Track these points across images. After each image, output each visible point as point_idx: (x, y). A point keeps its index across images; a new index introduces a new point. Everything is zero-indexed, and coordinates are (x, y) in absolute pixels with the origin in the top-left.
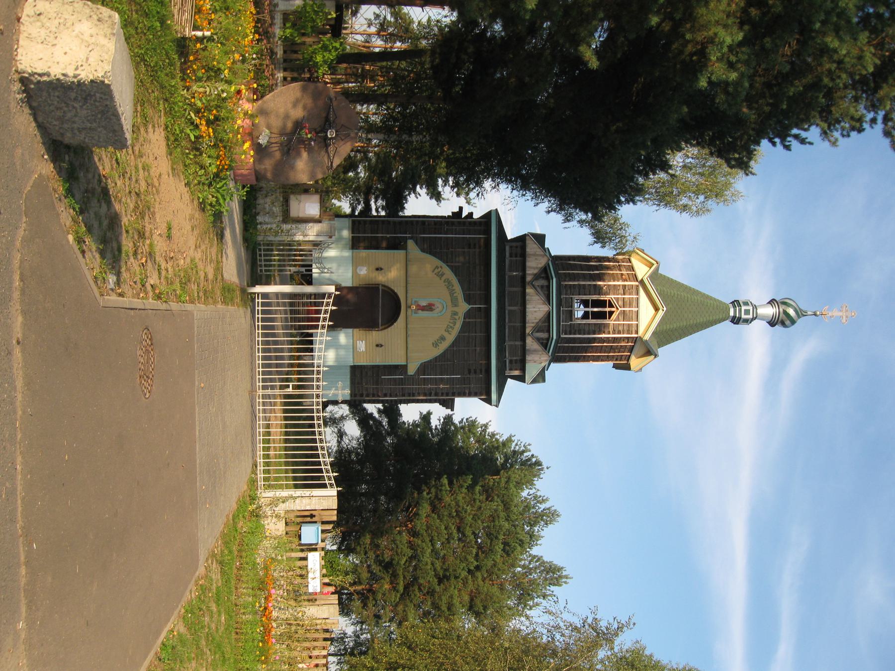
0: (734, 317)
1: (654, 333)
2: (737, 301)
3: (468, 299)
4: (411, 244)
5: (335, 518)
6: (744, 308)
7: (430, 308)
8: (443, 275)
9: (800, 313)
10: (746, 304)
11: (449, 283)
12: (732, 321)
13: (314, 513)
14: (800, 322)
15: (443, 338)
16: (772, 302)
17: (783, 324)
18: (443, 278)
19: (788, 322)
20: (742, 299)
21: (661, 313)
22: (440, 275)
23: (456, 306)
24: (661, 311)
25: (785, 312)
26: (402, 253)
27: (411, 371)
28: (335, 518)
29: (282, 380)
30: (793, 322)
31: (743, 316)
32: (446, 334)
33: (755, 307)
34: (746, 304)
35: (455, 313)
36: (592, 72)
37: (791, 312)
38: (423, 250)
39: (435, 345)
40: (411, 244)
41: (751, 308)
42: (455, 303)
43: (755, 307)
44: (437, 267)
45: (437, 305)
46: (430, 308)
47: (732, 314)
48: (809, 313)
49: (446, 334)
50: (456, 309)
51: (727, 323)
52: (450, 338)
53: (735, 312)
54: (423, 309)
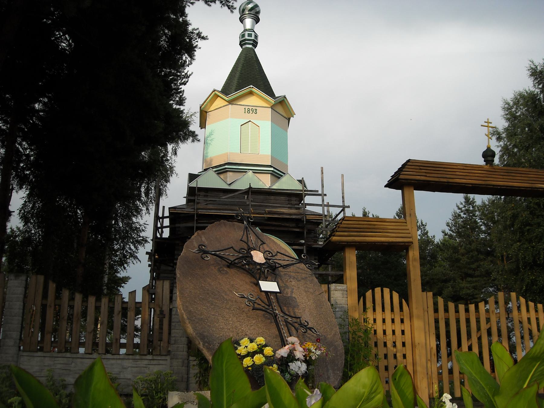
0: (252, 44)
2: (241, 42)
5: (41, 278)
12: (255, 47)
16: (242, 20)
17: (258, 12)
21: (255, 90)
28: (41, 278)
30: (256, 6)
33: (245, 30)
36: (80, 292)
37: (250, 6)
41: (247, 33)
43: (245, 30)
47: (251, 46)
48: (219, 102)
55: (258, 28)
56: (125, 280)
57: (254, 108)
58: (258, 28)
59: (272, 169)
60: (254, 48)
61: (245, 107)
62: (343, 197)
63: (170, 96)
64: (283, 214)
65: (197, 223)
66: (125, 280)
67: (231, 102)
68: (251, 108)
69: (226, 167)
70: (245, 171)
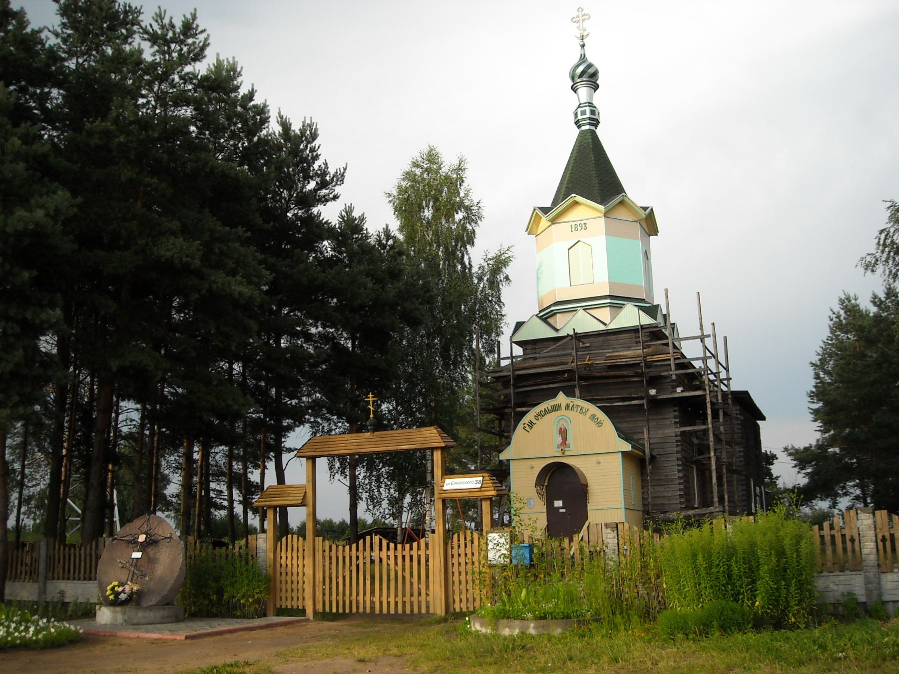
1: (601, 203)
3: (553, 394)
4: (503, 456)
6: (580, 117)
7: (563, 433)
8: (531, 422)
9: (583, 59)
10: (576, 114)
11: (539, 415)
13: (880, 537)
14: (591, 59)
15: (593, 417)
18: (534, 421)
19: (591, 71)
20: (573, 121)
21: (579, 198)
22: (531, 424)
23: (560, 406)
24: (576, 199)
25: (581, 75)
26: (513, 467)
27: (627, 447)
29: (22, 565)
30: (590, 66)
31: (588, 115)
32: (589, 414)
34: (576, 114)
35: (567, 407)
37: (581, 69)
38: (509, 443)
39: (599, 424)
40: (503, 456)
42: (556, 408)
44: (524, 428)
45: (560, 425)
46: (563, 433)
49: (589, 414)
50: (563, 407)
51: (600, 131)
52: (593, 409)
53: (585, 124)
54: (565, 439)
55: (598, 99)
56: (433, 195)
57: (582, 222)
58: (598, 99)
59: (608, 301)
60: (593, 128)
61: (570, 224)
62: (701, 325)
63: (868, 315)
64: (626, 357)
65: (515, 387)
66: (433, 195)
67: (553, 221)
68: (578, 223)
69: (552, 308)
70: (574, 310)
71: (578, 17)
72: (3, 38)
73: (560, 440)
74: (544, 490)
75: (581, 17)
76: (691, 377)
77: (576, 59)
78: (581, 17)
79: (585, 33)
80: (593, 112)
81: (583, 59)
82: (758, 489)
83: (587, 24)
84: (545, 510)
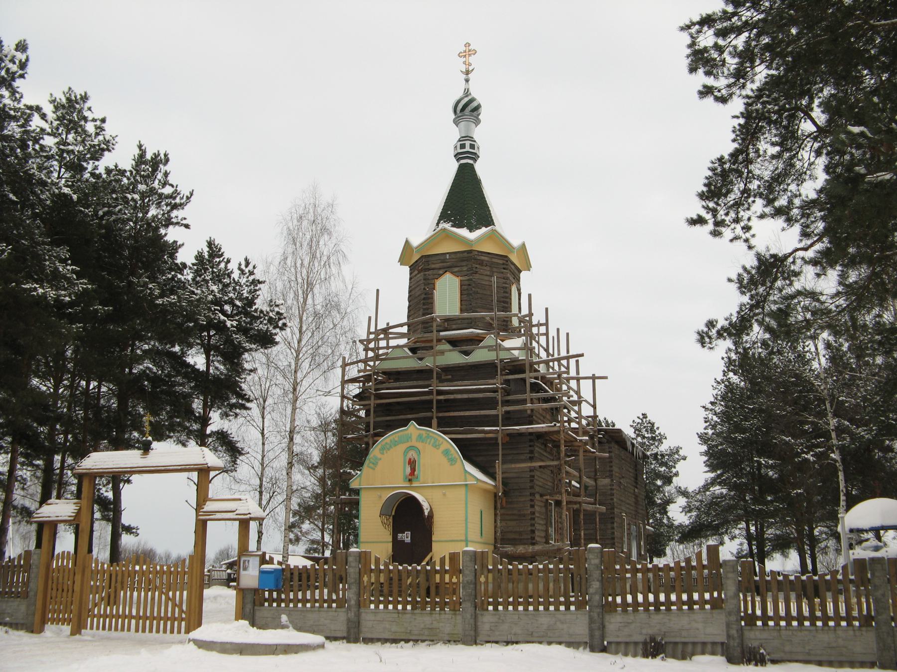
3: (405, 423)
7: (412, 463)
9: (467, 93)
14: (474, 94)
19: (474, 104)
30: (472, 100)
46: (412, 463)
54: (413, 470)
55: (479, 134)
71: (470, 55)
72: (892, 120)
73: (408, 470)
74: (391, 520)
75: (468, 52)
76: (726, 416)
77: (460, 94)
78: (468, 52)
79: (471, 69)
80: (472, 146)
81: (467, 93)
82: (633, 528)
83: (472, 59)
84: (433, 544)
